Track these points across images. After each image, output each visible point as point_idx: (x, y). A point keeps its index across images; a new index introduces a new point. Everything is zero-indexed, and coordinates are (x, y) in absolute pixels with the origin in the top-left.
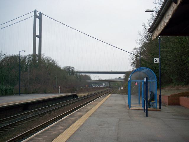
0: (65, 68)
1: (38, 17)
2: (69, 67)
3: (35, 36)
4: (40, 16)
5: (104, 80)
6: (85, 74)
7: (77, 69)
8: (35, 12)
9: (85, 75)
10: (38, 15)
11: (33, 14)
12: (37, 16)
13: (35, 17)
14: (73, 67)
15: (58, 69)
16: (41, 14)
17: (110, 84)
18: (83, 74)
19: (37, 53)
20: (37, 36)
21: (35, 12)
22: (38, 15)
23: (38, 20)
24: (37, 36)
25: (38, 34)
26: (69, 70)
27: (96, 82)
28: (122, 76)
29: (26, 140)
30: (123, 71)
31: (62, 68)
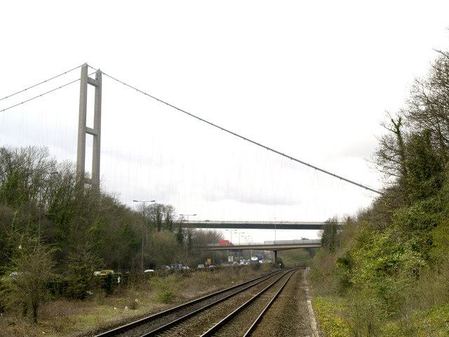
0: (145, 209)
1: (91, 81)
2: (160, 206)
3: (84, 130)
4: (97, 79)
5: (260, 246)
6: (209, 229)
7: (341, 219)
8: (85, 68)
9: (210, 233)
10: (93, 77)
11: (78, 74)
12: (89, 79)
13: (86, 80)
14: (171, 207)
15: (121, 211)
16: (99, 74)
17: (278, 256)
18: (204, 229)
19: (89, 168)
20: (90, 132)
21: (85, 68)
22: (93, 77)
23: (91, 90)
24: (90, 132)
25: (90, 124)
26: (159, 217)
27: (240, 251)
28: (314, 236)
29: (112, 313)
30: (309, 221)
31: (392, 180)
